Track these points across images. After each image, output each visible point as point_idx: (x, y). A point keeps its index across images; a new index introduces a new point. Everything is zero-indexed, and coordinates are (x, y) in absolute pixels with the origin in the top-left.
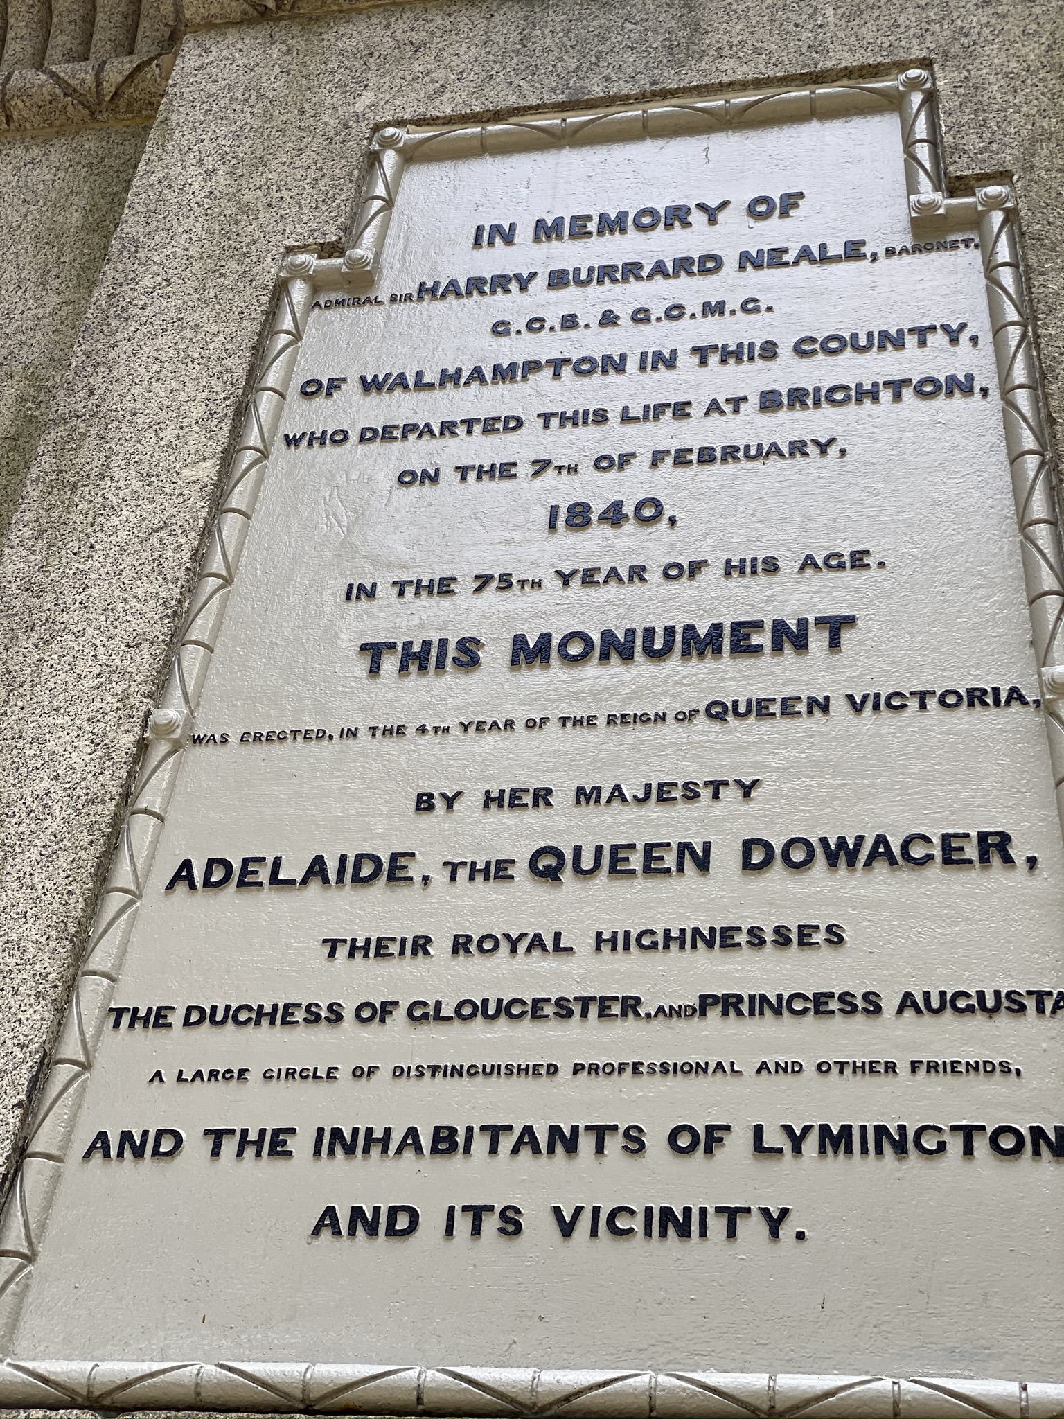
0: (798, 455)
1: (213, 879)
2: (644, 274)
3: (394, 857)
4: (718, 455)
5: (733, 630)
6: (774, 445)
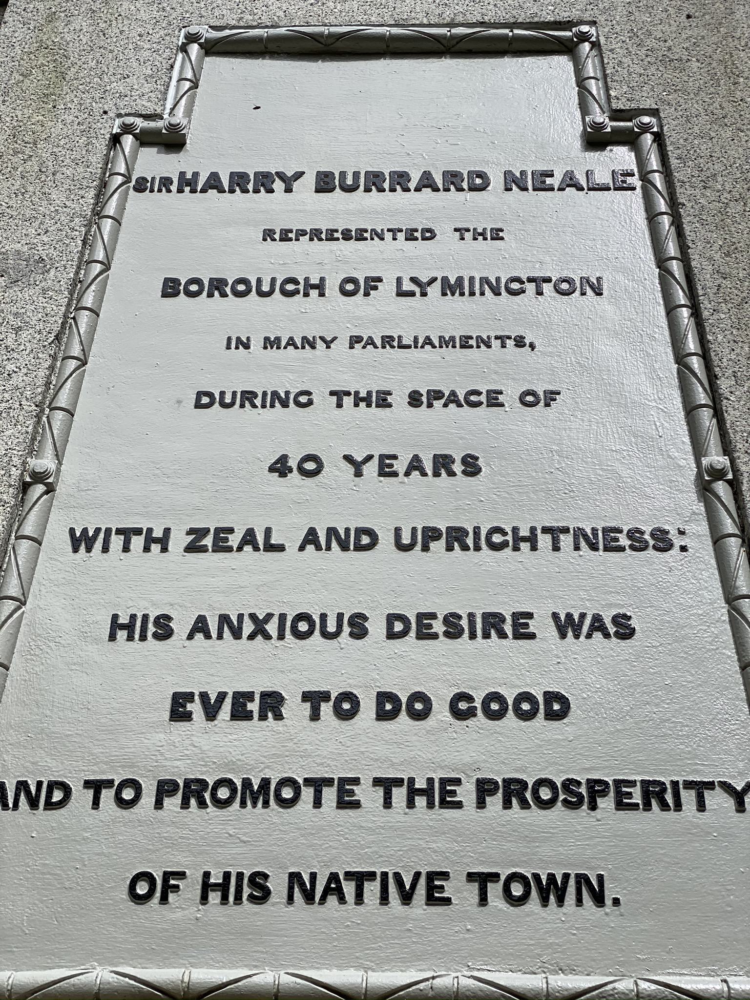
0: (388, 347)
1: (54, 800)
2: (412, 185)
3: (167, 876)
4: (424, 399)
5: (423, 531)
6: (370, 338)
